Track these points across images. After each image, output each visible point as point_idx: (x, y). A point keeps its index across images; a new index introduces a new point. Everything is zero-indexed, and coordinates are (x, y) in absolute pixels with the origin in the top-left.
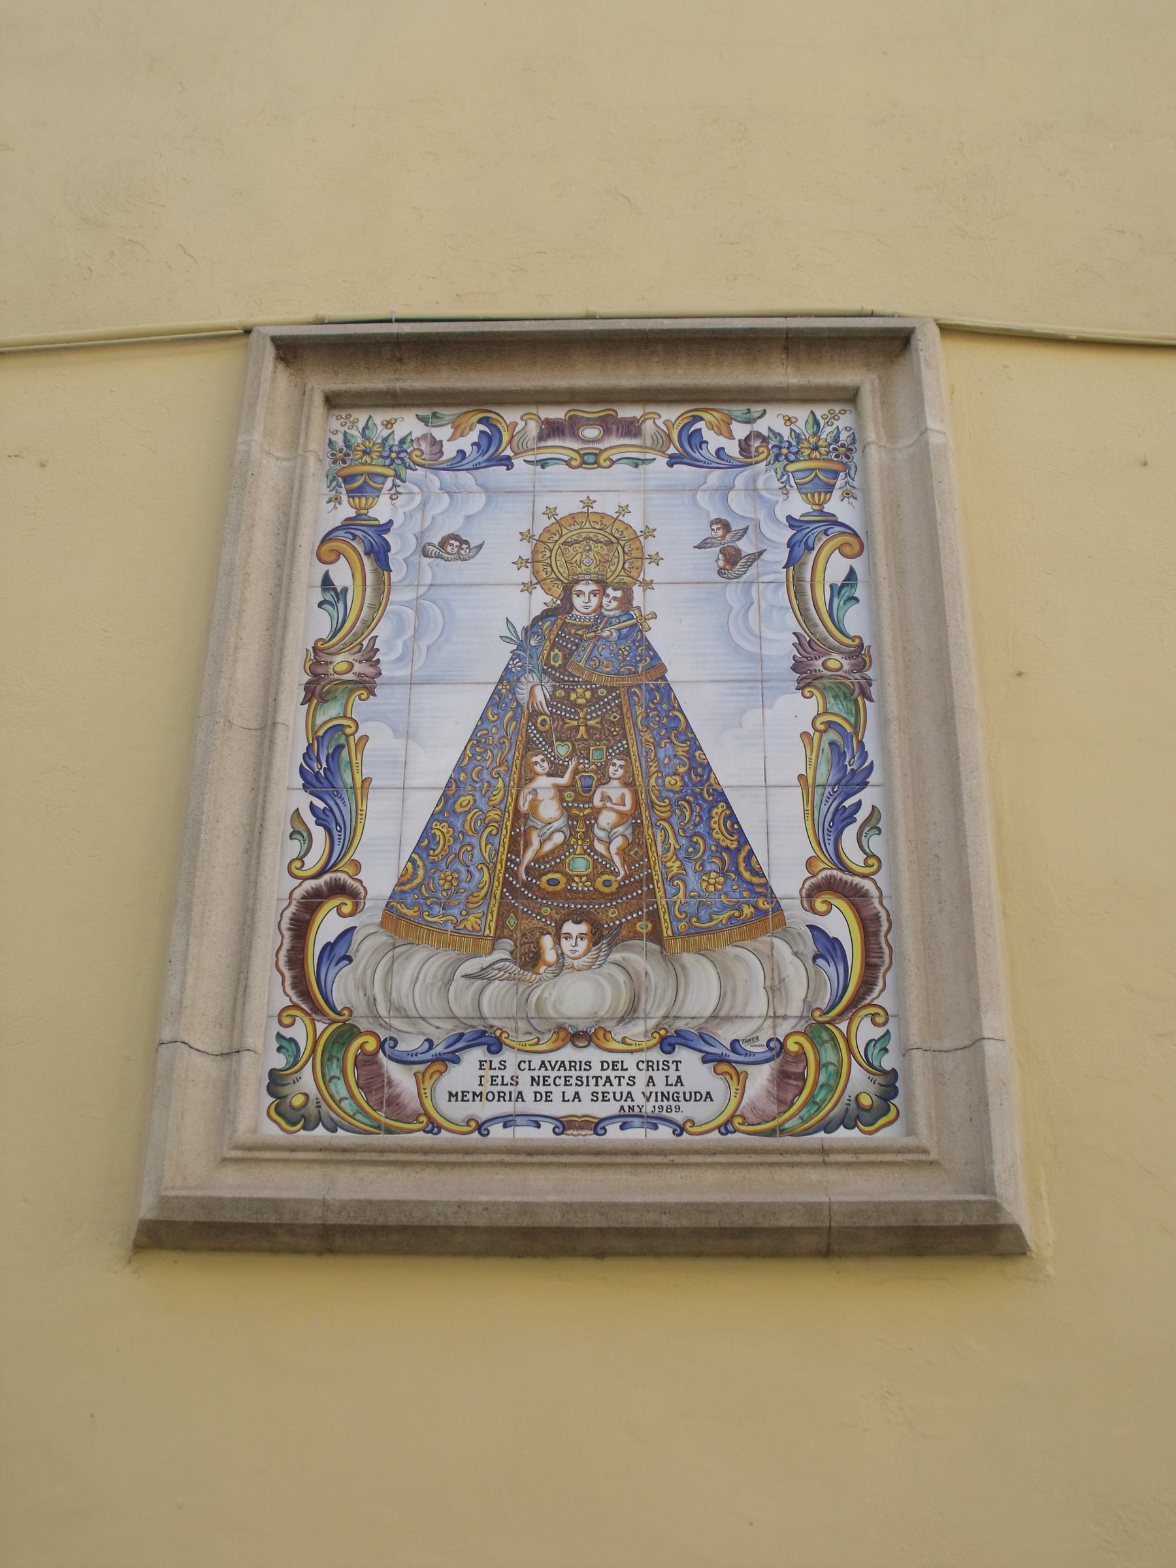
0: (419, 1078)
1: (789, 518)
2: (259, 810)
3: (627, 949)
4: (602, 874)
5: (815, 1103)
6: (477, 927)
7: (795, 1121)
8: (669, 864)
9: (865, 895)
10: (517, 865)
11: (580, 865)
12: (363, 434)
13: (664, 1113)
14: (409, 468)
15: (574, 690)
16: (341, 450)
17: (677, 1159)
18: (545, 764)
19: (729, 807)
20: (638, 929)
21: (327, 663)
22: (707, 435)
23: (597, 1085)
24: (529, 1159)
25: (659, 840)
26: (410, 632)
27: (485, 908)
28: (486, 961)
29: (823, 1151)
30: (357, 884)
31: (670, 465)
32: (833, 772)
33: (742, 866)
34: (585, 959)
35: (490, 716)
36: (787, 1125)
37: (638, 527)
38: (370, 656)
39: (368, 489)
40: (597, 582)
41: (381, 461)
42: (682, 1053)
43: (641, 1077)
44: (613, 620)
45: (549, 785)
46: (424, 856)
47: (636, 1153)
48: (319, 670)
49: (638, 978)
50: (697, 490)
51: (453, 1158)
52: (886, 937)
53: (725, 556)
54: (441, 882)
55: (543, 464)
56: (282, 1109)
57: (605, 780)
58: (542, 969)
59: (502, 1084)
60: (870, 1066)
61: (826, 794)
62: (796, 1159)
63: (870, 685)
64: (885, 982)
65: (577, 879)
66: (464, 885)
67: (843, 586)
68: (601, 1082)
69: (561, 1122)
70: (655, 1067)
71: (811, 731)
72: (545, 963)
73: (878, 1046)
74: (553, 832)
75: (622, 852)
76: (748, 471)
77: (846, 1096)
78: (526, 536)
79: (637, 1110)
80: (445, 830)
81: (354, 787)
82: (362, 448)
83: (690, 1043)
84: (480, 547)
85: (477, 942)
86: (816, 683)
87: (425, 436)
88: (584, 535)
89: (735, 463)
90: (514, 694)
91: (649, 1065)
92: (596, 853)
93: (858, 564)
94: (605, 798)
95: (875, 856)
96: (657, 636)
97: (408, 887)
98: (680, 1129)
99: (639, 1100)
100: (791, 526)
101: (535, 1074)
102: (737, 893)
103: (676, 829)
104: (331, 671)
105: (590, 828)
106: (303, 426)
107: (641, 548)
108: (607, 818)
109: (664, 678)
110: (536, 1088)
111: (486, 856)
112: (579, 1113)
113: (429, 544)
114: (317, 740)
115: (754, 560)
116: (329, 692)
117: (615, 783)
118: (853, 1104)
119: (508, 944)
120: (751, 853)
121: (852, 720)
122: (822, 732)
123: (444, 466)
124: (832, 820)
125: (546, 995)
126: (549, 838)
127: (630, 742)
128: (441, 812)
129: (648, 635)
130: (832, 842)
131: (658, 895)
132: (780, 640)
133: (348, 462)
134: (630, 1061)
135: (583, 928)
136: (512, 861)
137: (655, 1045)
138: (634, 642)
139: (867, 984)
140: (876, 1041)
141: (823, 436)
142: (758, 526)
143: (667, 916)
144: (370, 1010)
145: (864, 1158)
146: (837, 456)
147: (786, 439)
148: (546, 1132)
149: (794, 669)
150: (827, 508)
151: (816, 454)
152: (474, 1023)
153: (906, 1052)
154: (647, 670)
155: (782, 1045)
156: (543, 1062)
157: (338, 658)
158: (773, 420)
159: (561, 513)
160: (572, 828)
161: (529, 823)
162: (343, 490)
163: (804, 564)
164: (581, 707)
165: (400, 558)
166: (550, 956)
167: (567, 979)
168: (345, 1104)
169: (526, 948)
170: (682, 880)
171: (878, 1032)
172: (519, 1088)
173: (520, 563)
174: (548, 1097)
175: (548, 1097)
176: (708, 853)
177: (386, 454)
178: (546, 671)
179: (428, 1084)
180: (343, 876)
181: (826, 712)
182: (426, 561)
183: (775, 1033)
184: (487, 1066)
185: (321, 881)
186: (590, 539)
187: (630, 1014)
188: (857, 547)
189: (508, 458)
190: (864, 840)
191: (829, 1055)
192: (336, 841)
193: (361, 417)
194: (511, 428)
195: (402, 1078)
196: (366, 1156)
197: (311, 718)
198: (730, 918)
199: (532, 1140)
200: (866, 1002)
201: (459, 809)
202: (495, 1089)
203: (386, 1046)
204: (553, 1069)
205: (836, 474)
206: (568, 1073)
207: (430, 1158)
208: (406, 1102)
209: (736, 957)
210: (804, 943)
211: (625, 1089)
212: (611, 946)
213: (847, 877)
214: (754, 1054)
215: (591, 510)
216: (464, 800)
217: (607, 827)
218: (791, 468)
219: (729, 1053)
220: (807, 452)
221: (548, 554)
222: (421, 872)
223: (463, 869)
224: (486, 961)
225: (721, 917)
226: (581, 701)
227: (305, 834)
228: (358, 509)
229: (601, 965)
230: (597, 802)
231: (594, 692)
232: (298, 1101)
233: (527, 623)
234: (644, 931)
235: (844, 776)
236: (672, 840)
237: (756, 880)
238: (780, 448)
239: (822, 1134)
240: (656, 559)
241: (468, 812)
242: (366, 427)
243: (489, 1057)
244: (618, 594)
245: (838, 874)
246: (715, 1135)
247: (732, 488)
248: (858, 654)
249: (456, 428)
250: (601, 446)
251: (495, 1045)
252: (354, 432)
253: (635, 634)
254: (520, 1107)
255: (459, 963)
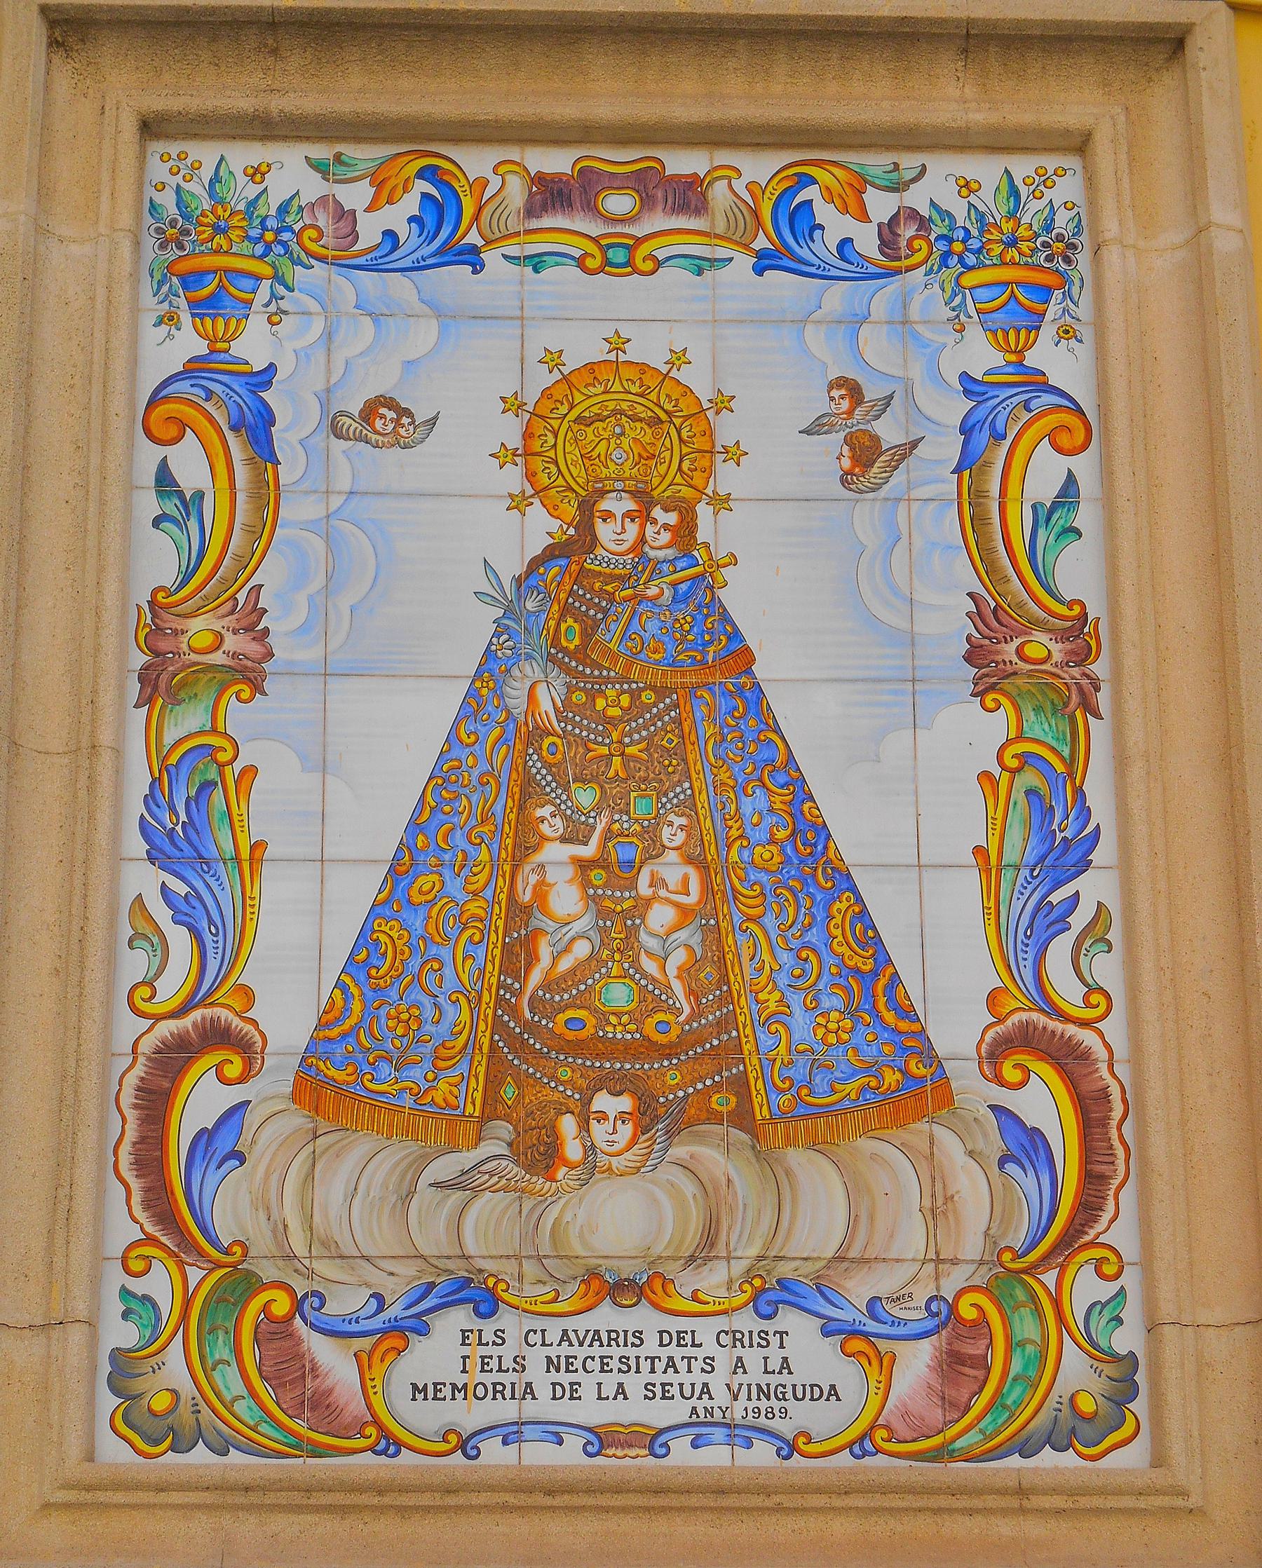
0: (363, 1363)
1: (965, 377)
2: (77, 900)
3: (701, 1139)
4: (655, 1010)
5: (1004, 1407)
6: (451, 1099)
7: (973, 1438)
8: (762, 996)
9: (1085, 1056)
10: (518, 994)
11: (619, 995)
12: (212, 193)
13: (762, 1420)
14: (298, 262)
15: (602, 693)
16: (173, 224)
17: (787, 1501)
18: (558, 822)
19: (859, 899)
20: (714, 1106)
21: (176, 632)
22: (824, 212)
23: (653, 1371)
24: (549, 1501)
25: (746, 955)
26: (318, 582)
27: (463, 1068)
28: (468, 1158)
29: (1021, 1491)
30: (248, 1027)
31: (759, 271)
32: (1033, 841)
33: (882, 1000)
34: (628, 1155)
35: (464, 736)
36: (958, 1444)
37: (704, 393)
38: (251, 621)
39: (227, 301)
40: (634, 494)
41: (246, 247)
42: (789, 1319)
43: (724, 1360)
44: (665, 567)
45: (565, 858)
46: (362, 978)
47: (722, 1492)
48: (163, 645)
49: (716, 1189)
50: (804, 321)
51: (426, 1500)
52: (1119, 1128)
53: (852, 449)
54: (391, 1023)
55: (536, 262)
56: (135, 1417)
57: (655, 850)
58: (561, 1172)
59: (500, 1370)
60: (1100, 1354)
61: (1020, 880)
62: (976, 1503)
63: (1097, 689)
64: (1117, 1204)
65: (613, 1019)
66: (428, 1028)
67: (1055, 506)
68: (660, 1366)
69: (596, 1434)
70: (746, 1341)
71: (996, 770)
72: (565, 1162)
73: (1107, 1314)
74: (573, 940)
75: (685, 972)
76: (894, 285)
77: (1054, 1396)
78: (512, 404)
79: (718, 1415)
80: (395, 935)
81: (237, 859)
82: (211, 219)
83: (802, 1301)
84: (433, 422)
85: (455, 1128)
86: (1006, 684)
87: (323, 200)
88: (611, 406)
89: (872, 269)
90: (501, 697)
91: (737, 1338)
92: (645, 975)
93: (1084, 466)
94: (656, 882)
95: (1101, 990)
96: (737, 596)
97: (335, 1032)
98: (789, 1448)
99: (721, 1397)
100: (967, 393)
101: (553, 1352)
102: (870, 1044)
103: (773, 936)
104: (185, 647)
105: (631, 934)
106: (105, 176)
107: (709, 433)
108: (660, 916)
109: (749, 672)
110: (554, 1376)
111: (465, 978)
112: (626, 1420)
113: (343, 413)
114: (164, 775)
115: (904, 457)
116: (183, 684)
117: (672, 856)
118: (1066, 1409)
119: (504, 1129)
120: (895, 979)
121: (1066, 753)
122: (1014, 772)
123: (361, 261)
124: (1031, 925)
125: (568, 1217)
126: (567, 949)
127: (696, 785)
128: (385, 902)
129: (721, 594)
130: (1029, 963)
131: (746, 1048)
132: (945, 611)
133: (189, 247)
134: (706, 1330)
135: (625, 1103)
136: (508, 988)
137: (746, 1304)
138: (699, 607)
139: (1089, 1207)
140: (1104, 1305)
141: (1026, 219)
142: (909, 392)
143: (760, 1084)
144: (279, 1246)
145: (1084, 1502)
146: (1049, 259)
147: (960, 223)
148: (571, 1453)
149: (969, 658)
150: (1031, 359)
151: (1013, 253)
152: (450, 1265)
153: (1152, 1328)
154: (721, 660)
155: (953, 1308)
156: (565, 1332)
157: (196, 624)
158: (938, 185)
159: (572, 362)
160: (604, 931)
161: (534, 923)
162: (182, 303)
163: (988, 464)
164: (611, 721)
165: (294, 437)
166: (573, 1150)
167: (601, 1188)
168: (239, 1407)
169: (533, 1137)
170: (784, 1024)
171: (1107, 1290)
172: (527, 1377)
173: (504, 456)
174: (573, 1392)
175: (573, 1392)
176: (825, 978)
177: (255, 233)
178: (556, 657)
179: (378, 1370)
180: (224, 1014)
181: (1020, 738)
182: (339, 445)
183: (938, 1289)
184: (473, 1338)
185: (187, 1022)
186: (622, 412)
187: (706, 1249)
188: (1080, 437)
189: (475, 250)
190: (1084, 962)
191: (1026, 1326)
192: (210, 953)
193: (206, 154)
194: (476, 188)
195: (335, 1362)
196: (283, 1498)
197: (153, 732)
198: (863, 1090)
199: (554, 1469)
200: (1087, 1238)
201: (417, 898)
202: (489, 1379)
203: (306, 1307)
204: (581, 1344)
205: (1049, 290)
206: (606, 1351)
207: (386, 1500)
208: (342, 1402)
209: (874, 1157)
210: (985, 1135)
211: (699, 1378)
212: (670, 1134)
213: (1058, 1026)
214: (906, 1322)
215: (622, 358)
216: (425, 882)
217: (661, 931)
218: (969, 280)
219: (864, 1320)
220: (997, 249)
221: (551, 441)
222: (356, 1006)
223: (427, 1001)
224: (468, 1158)
225: (848, 1088)
226: (614, 712)
227: (155, 940)
228: (213, 341)
229: (655, 1167)
230: (644, 889)
231: (635, 695)
232: (161, 1402)
233: (519, 569)
234: (724, 1109)
235: (1051, 850)
236: (766, 956)
237: (904, 1026)
238: (951, 241)
239: (1015, 1461)
240: (735, 454)
241: (432, 903)
242: (216, 179)
243: (477, 1324)
244: (672, 518)
245: (1040, 1019)
246: (845, 1458)
247: (865, 319)
248: (1077, 632)
249: (379, 185)
250: (638, 231)
251: (487, 1302)
252: (192, 187)
253: (701, 591)
254: (531, 1409)
255: (424, 1161)
